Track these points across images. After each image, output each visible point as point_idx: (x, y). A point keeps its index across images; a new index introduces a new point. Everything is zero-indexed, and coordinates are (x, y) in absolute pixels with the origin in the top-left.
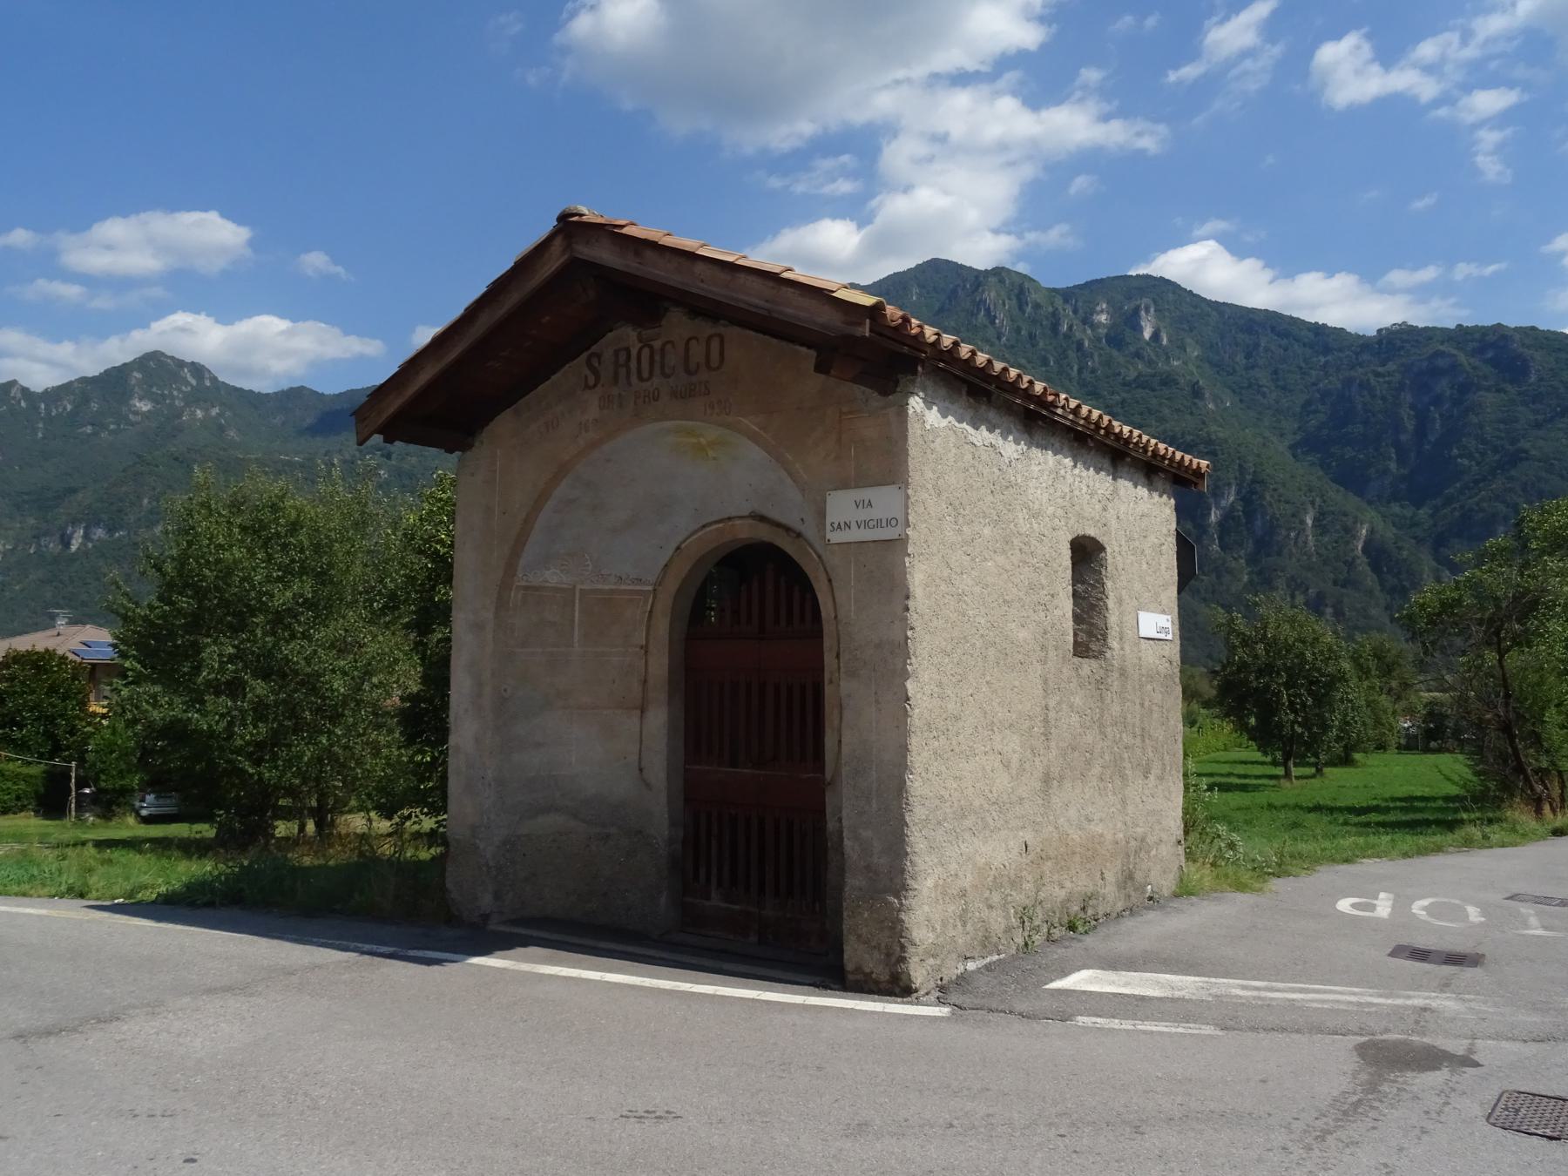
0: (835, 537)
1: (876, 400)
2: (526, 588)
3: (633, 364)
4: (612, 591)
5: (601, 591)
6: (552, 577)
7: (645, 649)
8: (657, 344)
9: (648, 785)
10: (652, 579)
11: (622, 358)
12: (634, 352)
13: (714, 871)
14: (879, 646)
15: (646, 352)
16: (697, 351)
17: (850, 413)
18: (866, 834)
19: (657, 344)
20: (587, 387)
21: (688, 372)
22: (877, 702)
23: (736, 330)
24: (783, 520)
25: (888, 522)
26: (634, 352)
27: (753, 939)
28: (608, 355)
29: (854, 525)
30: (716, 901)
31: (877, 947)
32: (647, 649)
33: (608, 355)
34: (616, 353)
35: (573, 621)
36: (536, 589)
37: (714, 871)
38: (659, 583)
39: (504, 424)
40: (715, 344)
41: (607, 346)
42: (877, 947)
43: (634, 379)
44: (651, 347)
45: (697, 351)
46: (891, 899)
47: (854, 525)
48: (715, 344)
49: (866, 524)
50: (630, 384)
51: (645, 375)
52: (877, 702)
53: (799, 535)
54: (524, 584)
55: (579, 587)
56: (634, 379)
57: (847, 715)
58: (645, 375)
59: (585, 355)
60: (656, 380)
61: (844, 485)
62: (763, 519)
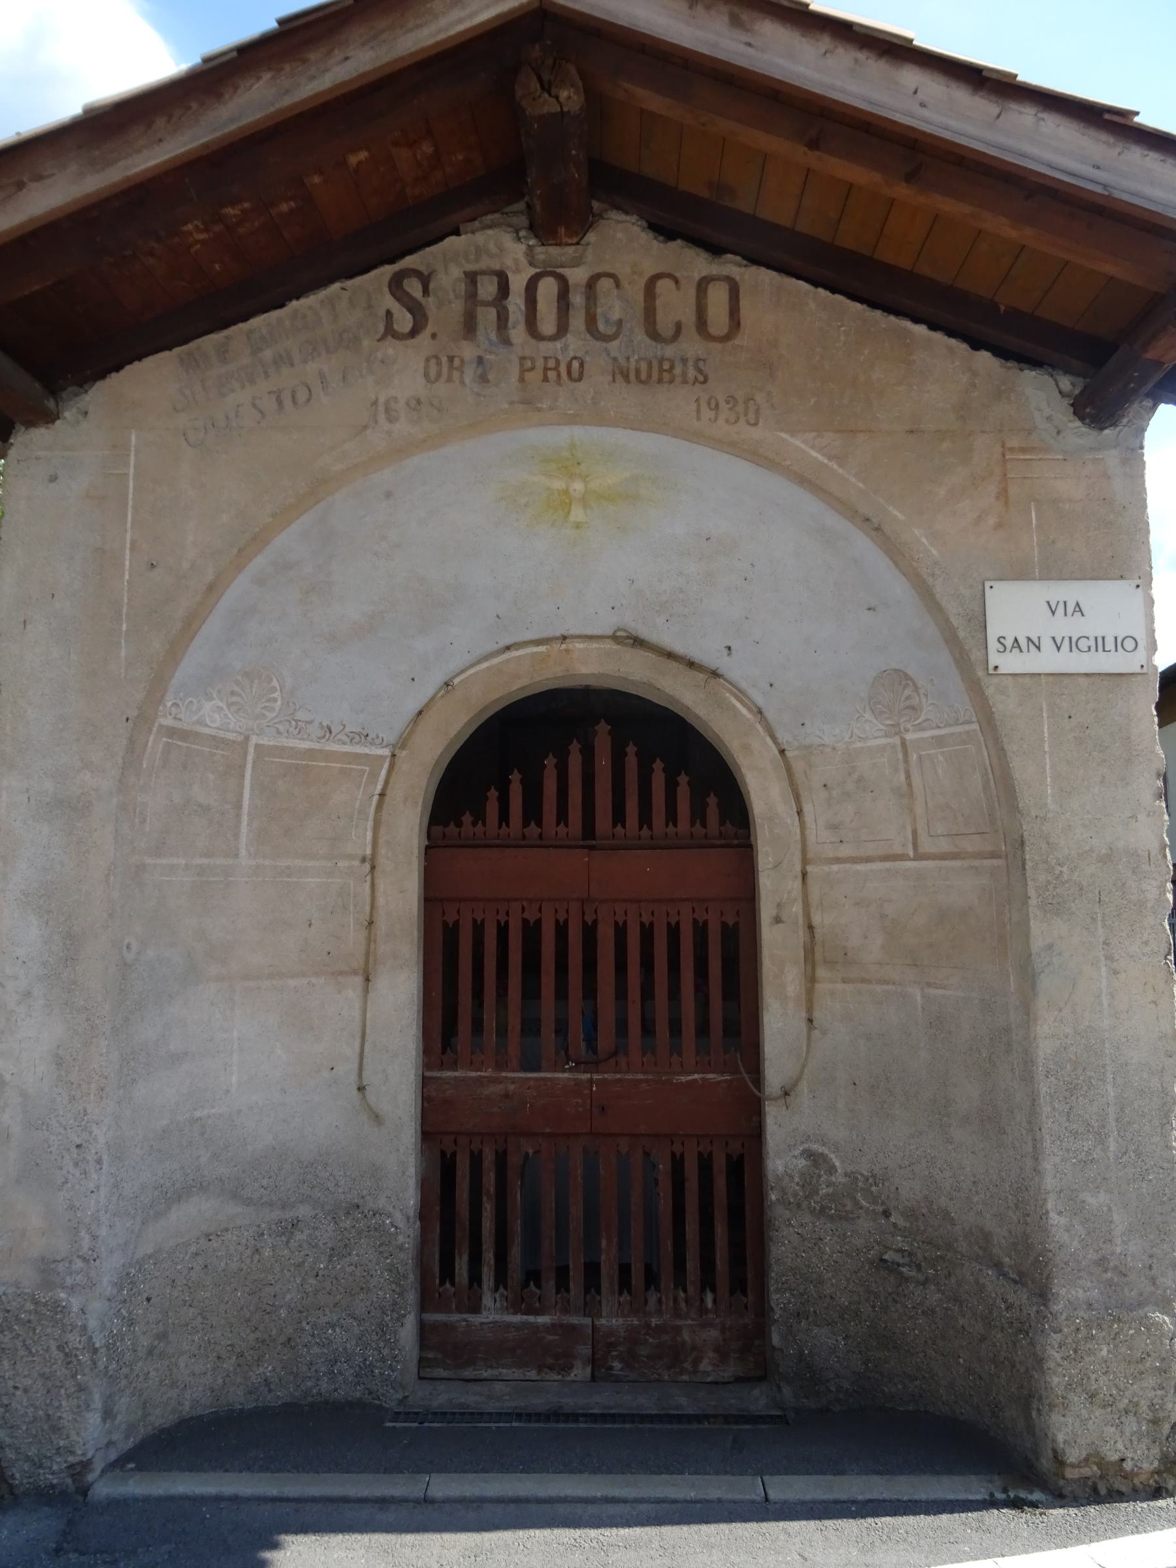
0: (1010, 663)
1: (1077, 433)
2: (172, 732)
3: (516, 303)
4: (310, 753)
5: (293, 752)
6: (212, 716)
7: (372, 863)
8: (577, 276)
9: (377, 1118)
10: (391, 737)
11: (487, 288)
12: (518, 283)
13: (489, 1256)
14: (1107, 859)
15: (547, 289)
16: (676, 304)
17: (1023, 450)
18: (1094, 1200)
19: (577, 276)
20: (390, 332)
21: (654, 334)
22: (1109, 958)
23: (766, 276)
24: (678, 647)
25: (1119, 643)
26: (518, 283)
27: (581, 1372)
28: (449, 278)
29: (1047, 644)
30: (493, 1312)
31: (1132, 1409)
32: (373, 869)
33: (449, 278)
34: (472, 278)
35: (238, 805)
36: (185, 735)
37: (489, 1256)
38: (403, 742)
39: (152, 379)
40: (718, 296)
41: (450, 260)
42: (1132, 1409)
43: (518, 333)
44: (563, 281)
45: (676, 304)
46: (1158, 1317)
47: (1047, 644)
48: (718, 296)
49: (1074, 644)
50: (507, 342)
51: (548, 326)
52: (1109, 958)
53: (715, 674)
54: (168, 722)
55: (254, 740)
56: (518, 333)
57: (1046, 983)
58: (548, 326)
59: (388, 270)
60: (576, 343)
61: (1020, 572)
62: (638, 642)
